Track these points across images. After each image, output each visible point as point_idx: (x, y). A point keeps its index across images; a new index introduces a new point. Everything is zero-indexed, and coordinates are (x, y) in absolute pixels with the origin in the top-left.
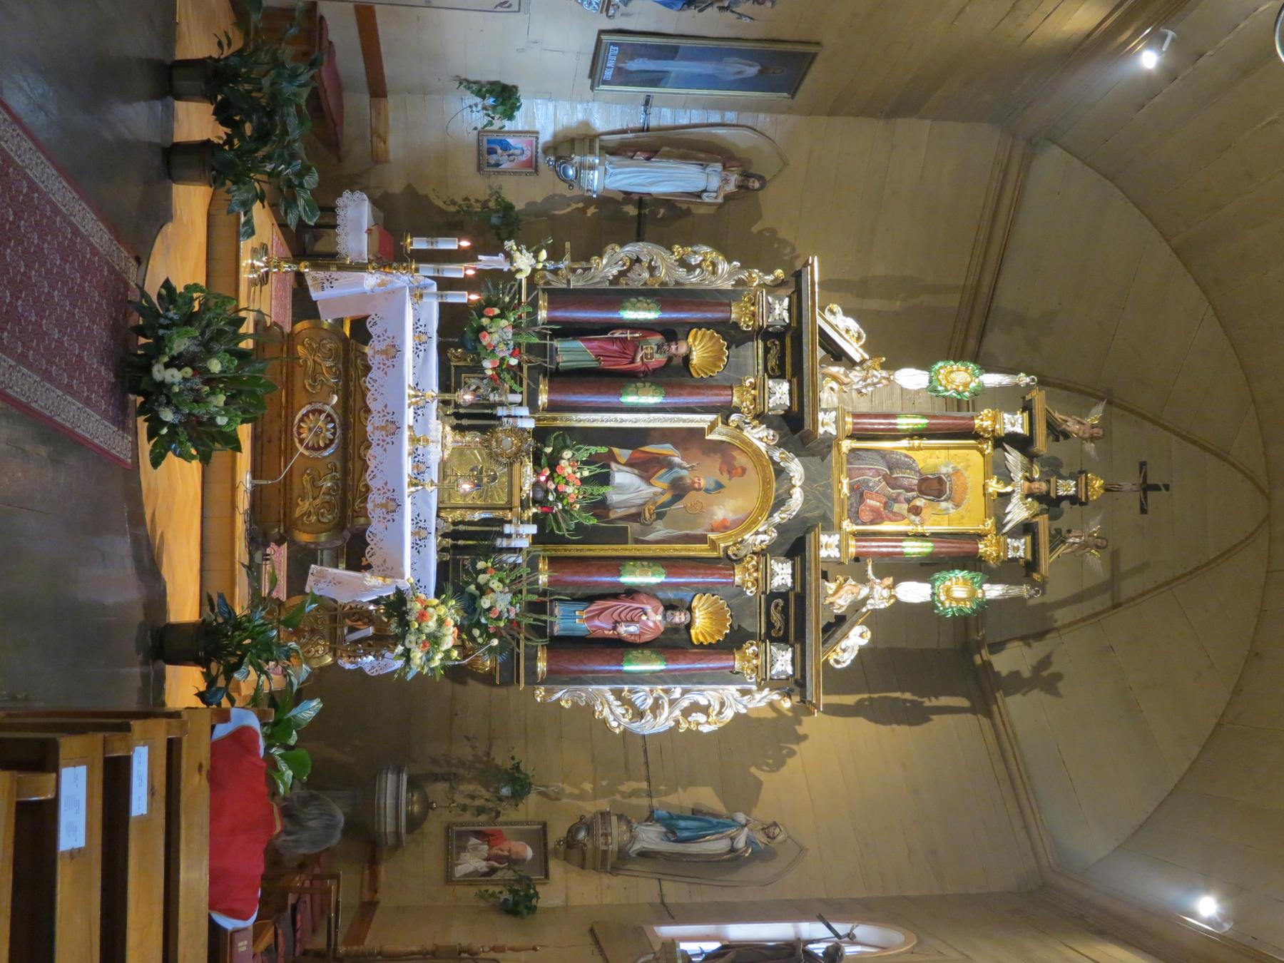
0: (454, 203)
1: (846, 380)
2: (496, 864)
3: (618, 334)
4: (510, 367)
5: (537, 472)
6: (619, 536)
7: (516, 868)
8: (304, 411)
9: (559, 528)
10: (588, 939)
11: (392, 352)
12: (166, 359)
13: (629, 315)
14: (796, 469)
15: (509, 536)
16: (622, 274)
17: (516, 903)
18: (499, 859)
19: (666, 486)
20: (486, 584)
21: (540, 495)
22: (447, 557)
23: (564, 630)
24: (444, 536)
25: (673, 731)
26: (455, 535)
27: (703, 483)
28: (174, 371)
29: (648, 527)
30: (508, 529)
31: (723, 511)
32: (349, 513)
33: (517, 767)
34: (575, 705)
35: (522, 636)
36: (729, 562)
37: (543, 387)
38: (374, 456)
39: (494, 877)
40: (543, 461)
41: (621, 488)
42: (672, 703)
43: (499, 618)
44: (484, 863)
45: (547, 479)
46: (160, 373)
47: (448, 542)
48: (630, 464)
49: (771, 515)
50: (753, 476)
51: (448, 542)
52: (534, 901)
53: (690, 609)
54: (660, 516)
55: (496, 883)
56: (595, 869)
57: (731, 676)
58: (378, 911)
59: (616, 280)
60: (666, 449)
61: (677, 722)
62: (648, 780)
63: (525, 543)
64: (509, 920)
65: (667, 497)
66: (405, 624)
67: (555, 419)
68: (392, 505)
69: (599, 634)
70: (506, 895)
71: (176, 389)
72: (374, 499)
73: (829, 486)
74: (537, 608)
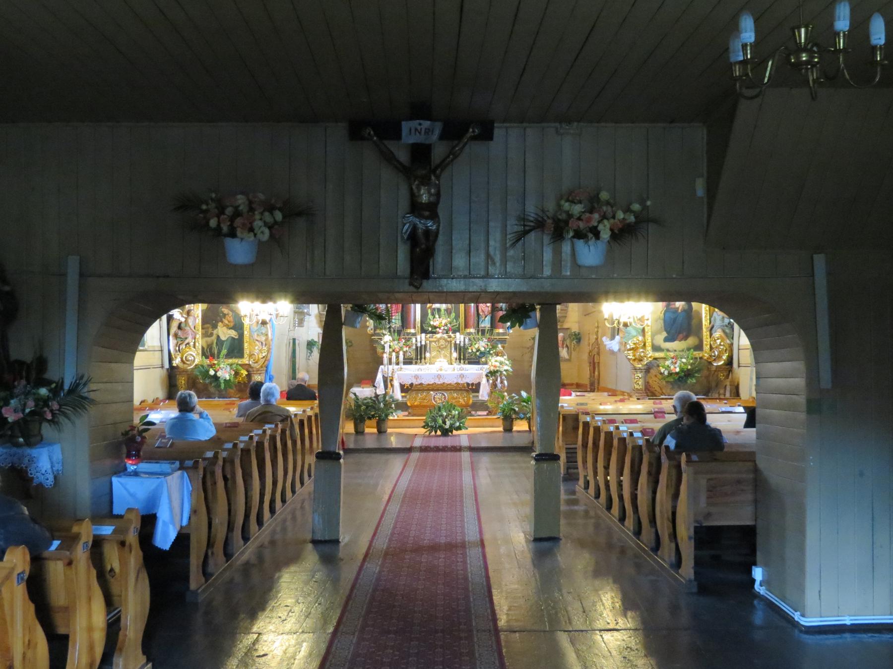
2: (565, 345)
4: (405, 342)
5: (439, 333)
7: (566, 338)
8: (434, 402)
9: (456, 325)
10: (587, 316)
11: (416, 377)
12: (444, 425)
15: (460, 342)
17: (577, 339)
18: (563, 344)
20: (476, 349)
21: (445, 332)
22: (467, 362)
23: (488, 323)
24: (460, 362)
26: (460, 359)
28: (447, 423)
30: (458, 342)
32: (463, 388)
35: (493, 337)
37: (409, 331)
38: (447, 381)
39: (569, 346)
40: (434, 330)
43: (488, 345)
44: (565, 349)
45: (440, 329)
46: (447, 426)
47: (462, 361)
51: (462, 361)
52: (576, 333)
55: (571, 345)
56: (566, 313)
58: (579, 382)
63: (462, 337)
64: (582, 341)
66: (497, 371)
67: (418, 327)
68: (462, 376)
70: (574, 342)
71: (452, 422)
72: (460, 381)
74: (483, 332)
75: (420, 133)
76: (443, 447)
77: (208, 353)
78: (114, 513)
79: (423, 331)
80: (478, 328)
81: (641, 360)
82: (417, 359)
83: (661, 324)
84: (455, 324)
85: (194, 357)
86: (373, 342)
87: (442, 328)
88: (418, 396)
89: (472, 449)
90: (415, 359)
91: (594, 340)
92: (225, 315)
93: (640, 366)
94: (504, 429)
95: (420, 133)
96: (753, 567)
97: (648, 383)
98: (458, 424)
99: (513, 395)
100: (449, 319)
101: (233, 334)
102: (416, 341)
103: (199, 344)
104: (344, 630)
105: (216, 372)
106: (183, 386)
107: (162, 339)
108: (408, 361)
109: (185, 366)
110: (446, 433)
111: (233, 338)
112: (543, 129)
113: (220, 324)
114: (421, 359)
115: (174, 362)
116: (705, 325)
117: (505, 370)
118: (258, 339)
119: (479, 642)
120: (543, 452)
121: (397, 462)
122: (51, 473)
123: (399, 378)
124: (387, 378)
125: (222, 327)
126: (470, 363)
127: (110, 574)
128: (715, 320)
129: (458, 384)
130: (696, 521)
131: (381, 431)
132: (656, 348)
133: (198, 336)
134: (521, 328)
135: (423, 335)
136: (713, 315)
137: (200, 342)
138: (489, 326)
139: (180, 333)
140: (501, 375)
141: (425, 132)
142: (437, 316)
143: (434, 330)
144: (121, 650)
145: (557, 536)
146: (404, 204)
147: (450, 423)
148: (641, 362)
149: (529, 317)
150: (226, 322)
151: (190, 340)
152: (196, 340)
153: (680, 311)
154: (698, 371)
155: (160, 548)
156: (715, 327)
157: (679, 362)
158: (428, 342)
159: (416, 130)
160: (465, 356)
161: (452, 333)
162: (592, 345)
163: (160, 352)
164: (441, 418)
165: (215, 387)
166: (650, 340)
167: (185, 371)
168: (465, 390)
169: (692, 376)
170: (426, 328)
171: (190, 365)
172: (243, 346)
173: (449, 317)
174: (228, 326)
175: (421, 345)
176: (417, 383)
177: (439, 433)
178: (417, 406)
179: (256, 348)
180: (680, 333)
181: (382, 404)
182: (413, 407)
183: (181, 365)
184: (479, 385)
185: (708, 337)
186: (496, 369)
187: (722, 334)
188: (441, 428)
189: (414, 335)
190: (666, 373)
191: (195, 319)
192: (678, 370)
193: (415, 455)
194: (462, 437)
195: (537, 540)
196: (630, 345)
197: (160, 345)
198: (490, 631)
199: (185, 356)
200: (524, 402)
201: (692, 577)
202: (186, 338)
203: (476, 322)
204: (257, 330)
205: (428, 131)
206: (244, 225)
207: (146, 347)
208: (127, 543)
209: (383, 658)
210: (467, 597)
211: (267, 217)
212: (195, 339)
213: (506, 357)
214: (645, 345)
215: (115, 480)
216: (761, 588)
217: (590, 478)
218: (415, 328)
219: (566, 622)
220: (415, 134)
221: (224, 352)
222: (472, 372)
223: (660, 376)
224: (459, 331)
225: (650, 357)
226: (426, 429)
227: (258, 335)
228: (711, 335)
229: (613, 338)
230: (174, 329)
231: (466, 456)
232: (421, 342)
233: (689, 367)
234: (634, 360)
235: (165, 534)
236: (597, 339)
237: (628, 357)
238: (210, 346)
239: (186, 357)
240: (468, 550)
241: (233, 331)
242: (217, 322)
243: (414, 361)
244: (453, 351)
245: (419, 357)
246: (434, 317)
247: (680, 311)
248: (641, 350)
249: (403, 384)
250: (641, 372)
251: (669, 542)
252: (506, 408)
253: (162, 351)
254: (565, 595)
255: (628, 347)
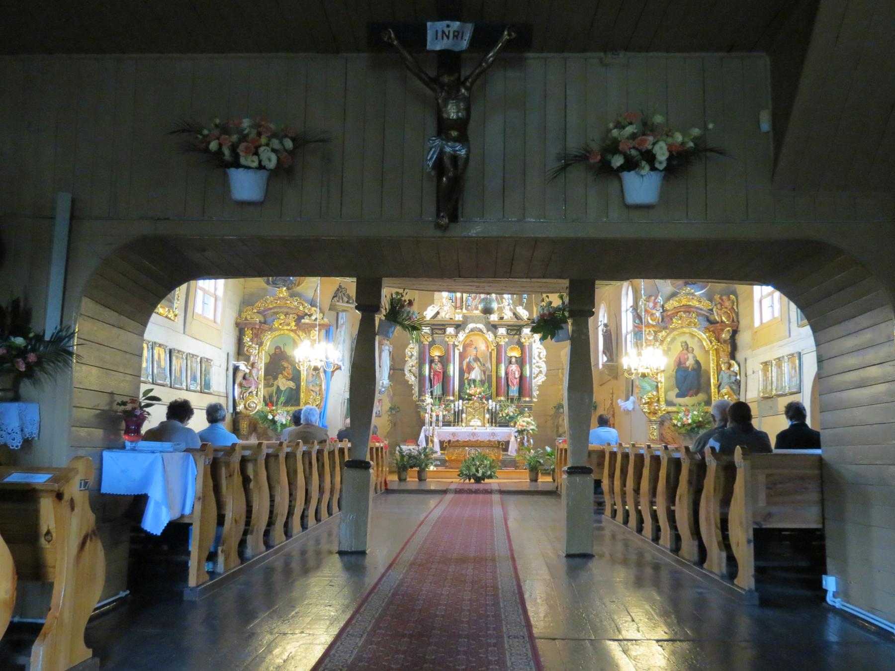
0: (389, 425)
1: (447, 311)
3: (432, 376)
6: (490, 377)
9: (489, 394)
10: (603, 386)
11: (454, 434)
13: (427, 373)
14: (471, 326)
15: (492, 408)
16: (414, 375)
19: (475, 363)
22: (498, 425)
24: (492, 425)
25: (546, 362)
27: (475, 353)
29: (487, 368)
30: (490, 408)
31: (482, 347)
33: (555, 407)
34: (538, 390)
36: (498, 346)
40: (470, 398)
41: (476, 376)
42: (537, 362)
43: (516, 411)
46: (480, 475)
47: (494, 424)
48: (469, 373)
49: (484, 333)
50: (473, 338)
51: (494, 424)
53: (511, 357)
54: (484, 365)
57: (530, 346)
59: (416, 377)
60: (465, 363)
61: (543, 361)
62: (559, 369)
64: (597, 408)
65: (479, 363)
69: (518, 383)
72: (492, 439)
73: (476, 316)
74: (512, 400)
75: (448, 37)
76: (476, 490)
77: (269, 401)
78: (102, 492)
79: (460, 398)
80: (508, 396)
81: (655, 413)
82: (455, 422)
83: (673, 381)
84: (488, 393)
85: (256, 404)
86: (418, 406)
87: (477, 396)
88: (455, 451)
89: (502, 492)
90: (453, 422)
91: (609, 405)
92: (284, 368)
93: (654, 418)
94: (530, 480)
95: (448, 37)
96: (824, 576)
97: (662, 434)
98: (489, 473)
99: (539, 449)
100: (482, 389)
101: (291, 384)
102: (455, 406)
103: (261, 393)
104: (350, 633)
105: (274, 416)
106: (245, 430)
107: (227, 387)
108: (447, 424)
109: (248, 412)
110: (478, 480)
111: (290, 388)
112: (586, 60)
113: (280, 376)
114: (458, 422)
115: (238, 408)
116: (714, 382)
117: (531, 429)
118: (313, 389)
119: (512, 650)
120: (575, 465)
121: (433, 501)
122: (19, 433)
123: (439, 435)
124: (428, 437)
125: (282, 379)
126: (500, 426)
127: (46, 537)
128: (722, 378)
129: (489, 441)
130: (756, 523)
131: (421, 479)
132: (669, 403)
133: (260, 386)
134: (553, 340)
135: (461, 401)
136: (720, 373)
137: (262, 392)
138: (517, 395)
139: (244, 382)
140: (527, 434)
141: (454, 36)
142: (473, 386)
143: (470, 398)
144: (45, 635)
145: (591, 553)
146: (432, 127)
147: (483, 472)
148: (656, 415)
149: (562, 328)
150: (286, 374)
151: (253, 388)
152: (259, 389)
153: (690, 370)
154: (709, 422)
155: (149, 532)
156: (722, 384)
157: (691, 414)
158: (465, 407)
159: (443, 32)
160: (495, 419)
161: (486, 400)
162: (607, 410)
163: (226, 398)
164: (475, 467)
165: (272, 430)
166: (663, 395)
167: (248, 416)
168: (495, 447)
169: (703, 427)
170: (463, 396)
171: (252, 411)
172: (300, 395)
173: (482, 387)
174: (287, 377)
175: (459, 410)
176: (454, 440)
177: (472, 481)
178: (454, 460)
179: (312, 397)
180: (690, 389)
181: (422, 455)
182: (451, 461)
183: (244, 411)
184: (508, 443)
185: (717, 393)
186: (523, 428)
187: (729, 390)
188: (474, 475)
189: (453, 401)
190: (679, 424)
191: (258, 371)
192: (690, 421)
193: (449, 497)
194: (493, 483)
195: (568, 556)
196: (645, 399)
197: (225, 391)
198: (524, 638)
199: (248, 402)
200: (548, 455)
201: (753, 586)
202: (250, 387)
203: (506, 392)
204: (313, 381)
205: (457, 35)
206: (247, 148)
207: (211, 391)
208: (66, 497)
209: (391, 664)
210: (496, 604)
211: (275, 143)
212: (257, 389)
213: (531, 418)
214: (658, 400)
215: (106, 455)
216: (836, 600)
217: (619, 507)
218: (453, 395)
219: (614, 631)
220: (443, 38)
221: (282, 399)
222: (501, 433)
223: (673, 428)
224: (491, 399)
225: (664, 410)
226: (461, 477)
227: (313, 386)
228: (719, 391)
229: (627, 399)
230: (239, 379)
231: (496, 497)
232: (458, 407)
233: (701, 419)
234: (649, 413)
235: (157, 516)
236: (612, 404)
237: (644, 410)
238: (271, 396)
239: (249, 404)
240: (497, 563)
241: (291, 382)
242: (278, 374)
243: (452, 424)
244: (486, 413)
245: (456, 421)
246: (470, 386)
247: (690, 370)
248: (656, 404)
249: (442, 440)
250: (656, 424)
251: (719, 551)
252: (532, 461)
253: (227, 397)
254: (608, 603)
255: (644, 401)
